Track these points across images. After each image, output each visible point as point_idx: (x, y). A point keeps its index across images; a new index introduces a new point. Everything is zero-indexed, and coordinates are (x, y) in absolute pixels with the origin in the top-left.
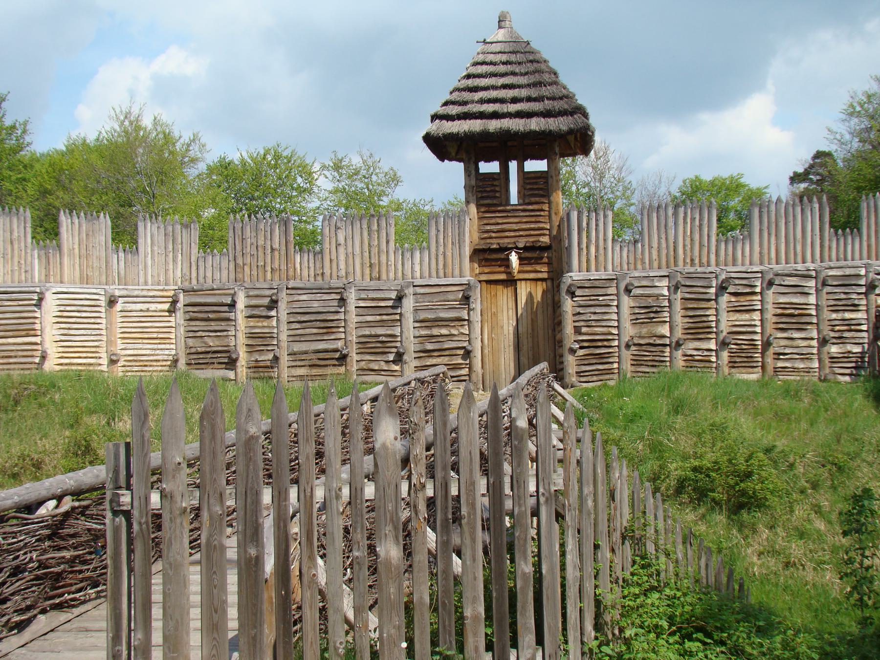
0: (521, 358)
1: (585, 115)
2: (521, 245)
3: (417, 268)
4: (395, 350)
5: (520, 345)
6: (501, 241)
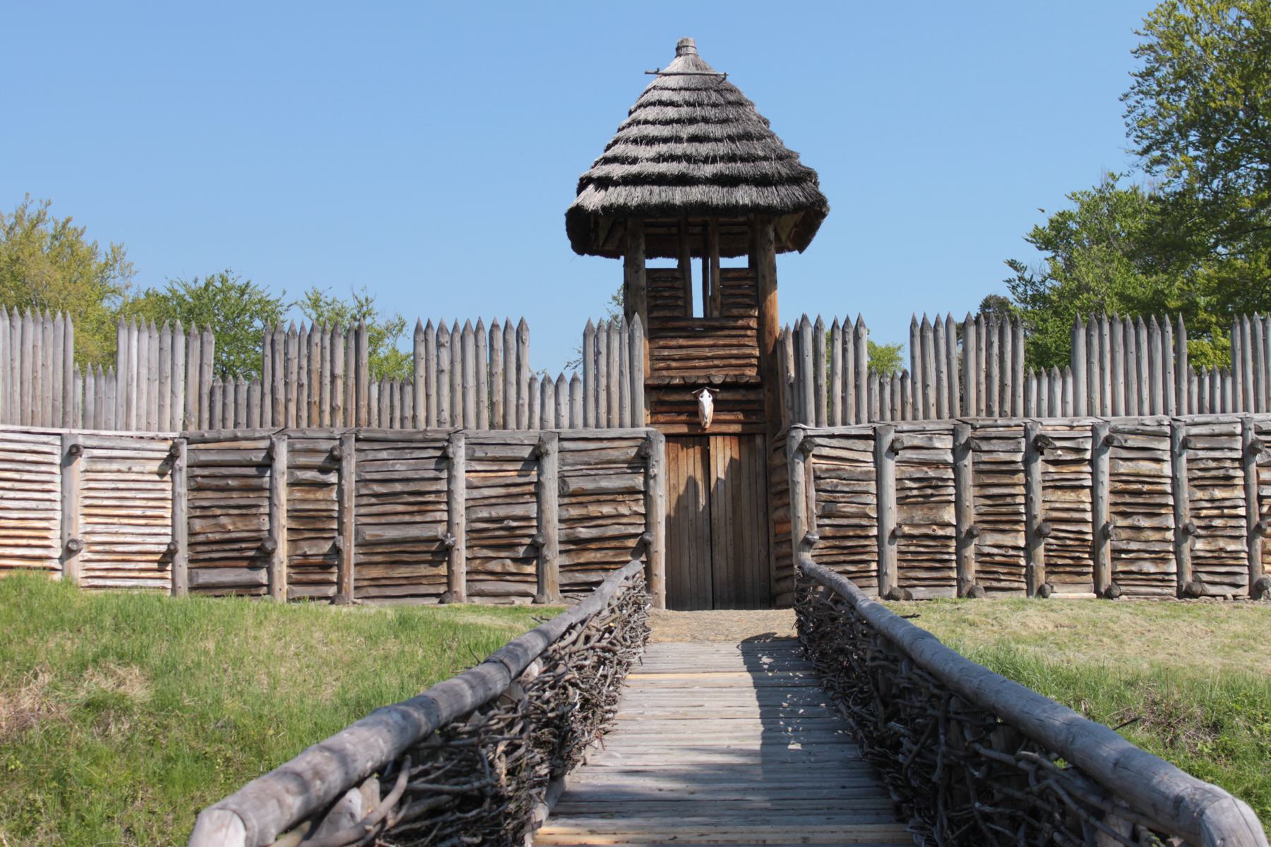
0: (716, 557)
1: (816, 184)
2: (718, 380)
3: (565, 410)
4: (528, 541)
5: (715, 536)
6: (686, 374)
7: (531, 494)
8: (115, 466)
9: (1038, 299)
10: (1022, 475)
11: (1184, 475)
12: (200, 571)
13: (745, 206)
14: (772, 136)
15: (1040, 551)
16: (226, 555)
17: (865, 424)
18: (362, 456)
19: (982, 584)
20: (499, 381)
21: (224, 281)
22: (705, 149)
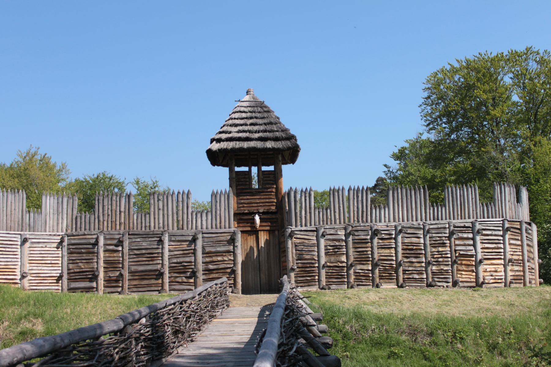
0: (262, 275)
1: (296, 140)
2: (261, 211)
4: (191, 270)
5: (261, 267)
6: (250, 209)
7: (192, 253)
8: (40, 245)
9: (395, 178)
10: (370, 244)
11: (428, 243)
12: (72, 283)
13: (270, 148)
14: (280, 123)
15: (377, 271)
16: (81, 277)
17: (313, 226)
18: (131, 240)
19: (356, 283)
20: (180, 212)
21: (104, 175)
22: (256, 128)
